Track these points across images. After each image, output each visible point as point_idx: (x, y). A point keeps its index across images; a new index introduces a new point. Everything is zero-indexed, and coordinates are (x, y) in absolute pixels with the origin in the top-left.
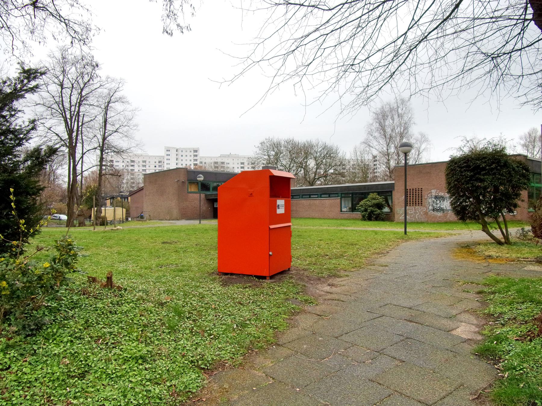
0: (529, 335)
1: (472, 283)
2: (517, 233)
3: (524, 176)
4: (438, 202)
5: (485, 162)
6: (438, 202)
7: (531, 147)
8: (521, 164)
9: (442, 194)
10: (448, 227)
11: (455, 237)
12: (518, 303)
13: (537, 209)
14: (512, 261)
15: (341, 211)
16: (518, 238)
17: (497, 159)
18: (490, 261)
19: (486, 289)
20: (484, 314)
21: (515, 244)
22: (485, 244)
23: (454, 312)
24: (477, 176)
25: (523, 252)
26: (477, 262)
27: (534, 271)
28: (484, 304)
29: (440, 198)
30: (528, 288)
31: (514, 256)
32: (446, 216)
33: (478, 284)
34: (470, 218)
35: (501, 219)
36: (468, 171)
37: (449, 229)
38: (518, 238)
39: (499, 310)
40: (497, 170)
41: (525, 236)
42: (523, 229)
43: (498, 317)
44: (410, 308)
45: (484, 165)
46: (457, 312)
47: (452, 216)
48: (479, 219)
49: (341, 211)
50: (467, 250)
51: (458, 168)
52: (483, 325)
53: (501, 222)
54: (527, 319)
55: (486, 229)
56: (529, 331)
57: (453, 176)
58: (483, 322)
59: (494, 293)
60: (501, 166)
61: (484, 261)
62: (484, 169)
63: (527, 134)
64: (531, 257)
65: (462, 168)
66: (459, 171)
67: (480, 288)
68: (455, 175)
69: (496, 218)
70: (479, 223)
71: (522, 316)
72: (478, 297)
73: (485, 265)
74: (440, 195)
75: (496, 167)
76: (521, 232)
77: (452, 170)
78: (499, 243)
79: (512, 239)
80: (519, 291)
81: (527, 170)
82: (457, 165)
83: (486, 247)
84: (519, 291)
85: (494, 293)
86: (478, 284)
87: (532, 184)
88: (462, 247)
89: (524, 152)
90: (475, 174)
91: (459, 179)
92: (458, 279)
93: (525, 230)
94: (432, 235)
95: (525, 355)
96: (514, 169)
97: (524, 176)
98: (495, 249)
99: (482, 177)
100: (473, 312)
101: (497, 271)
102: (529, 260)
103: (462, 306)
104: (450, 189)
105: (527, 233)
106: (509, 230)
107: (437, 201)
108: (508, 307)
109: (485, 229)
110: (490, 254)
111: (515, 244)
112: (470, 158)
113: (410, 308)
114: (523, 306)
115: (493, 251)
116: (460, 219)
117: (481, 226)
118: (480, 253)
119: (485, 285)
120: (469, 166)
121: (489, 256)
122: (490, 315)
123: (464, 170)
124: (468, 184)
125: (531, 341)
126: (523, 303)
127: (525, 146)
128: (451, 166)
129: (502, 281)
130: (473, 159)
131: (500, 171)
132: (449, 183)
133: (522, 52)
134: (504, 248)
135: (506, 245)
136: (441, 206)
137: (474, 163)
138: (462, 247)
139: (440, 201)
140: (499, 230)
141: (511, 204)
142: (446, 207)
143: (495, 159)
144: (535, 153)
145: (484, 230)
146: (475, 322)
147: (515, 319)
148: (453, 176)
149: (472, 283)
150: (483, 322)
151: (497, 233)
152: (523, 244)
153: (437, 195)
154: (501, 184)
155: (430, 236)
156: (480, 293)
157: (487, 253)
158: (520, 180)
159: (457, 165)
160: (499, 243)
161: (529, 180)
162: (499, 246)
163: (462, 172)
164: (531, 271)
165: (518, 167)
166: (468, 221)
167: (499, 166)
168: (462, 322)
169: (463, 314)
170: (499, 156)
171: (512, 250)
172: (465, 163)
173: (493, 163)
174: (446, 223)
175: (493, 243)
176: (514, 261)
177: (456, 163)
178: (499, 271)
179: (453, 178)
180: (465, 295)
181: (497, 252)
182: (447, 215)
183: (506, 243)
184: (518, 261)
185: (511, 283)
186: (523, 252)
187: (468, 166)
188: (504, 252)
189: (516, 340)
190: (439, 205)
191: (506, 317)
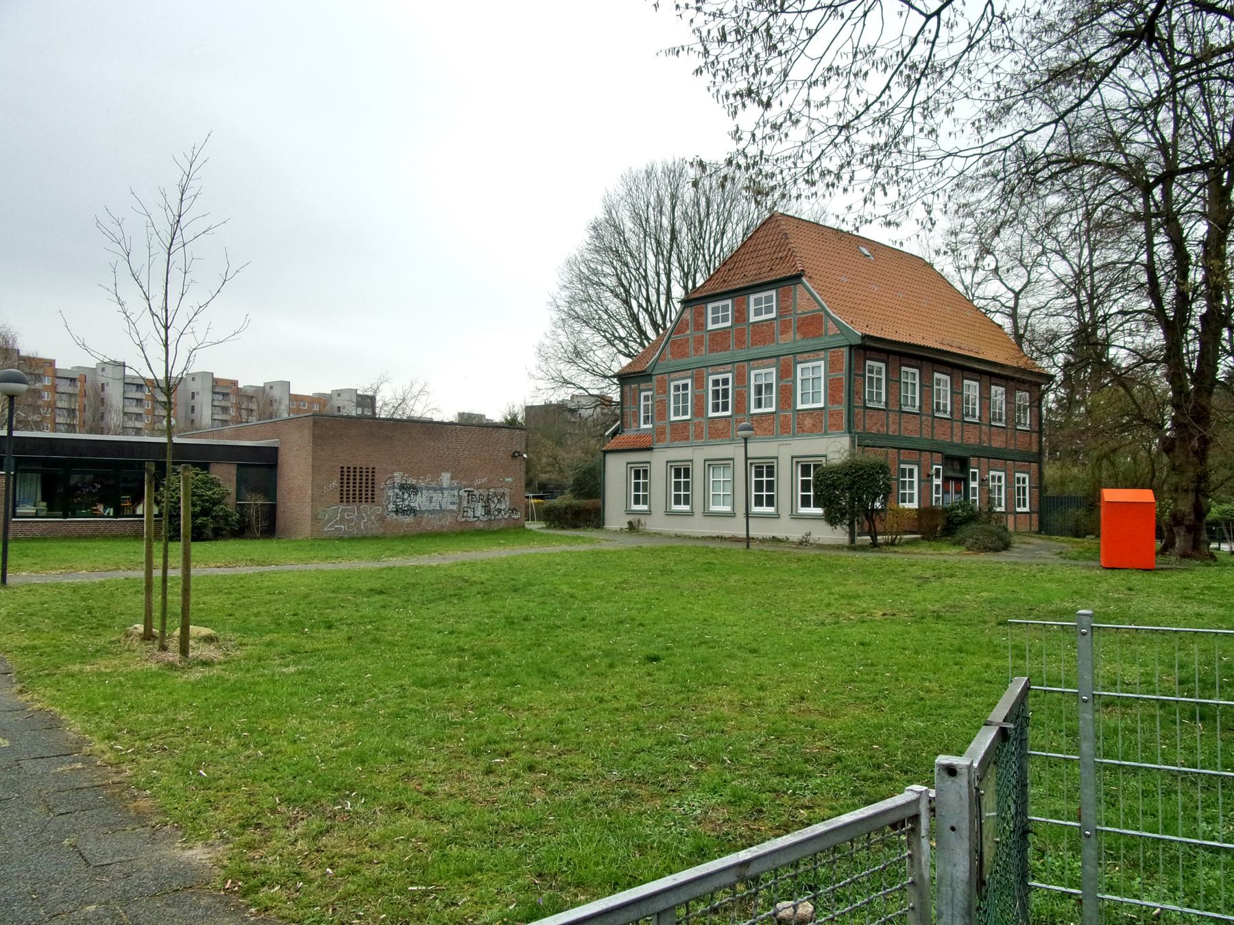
4: (406, 496)
6: (406, 496)
9: (414, 482)
32: (419, 523)
136: (412, 505)
139: (410, 496)
190: (406, 503)
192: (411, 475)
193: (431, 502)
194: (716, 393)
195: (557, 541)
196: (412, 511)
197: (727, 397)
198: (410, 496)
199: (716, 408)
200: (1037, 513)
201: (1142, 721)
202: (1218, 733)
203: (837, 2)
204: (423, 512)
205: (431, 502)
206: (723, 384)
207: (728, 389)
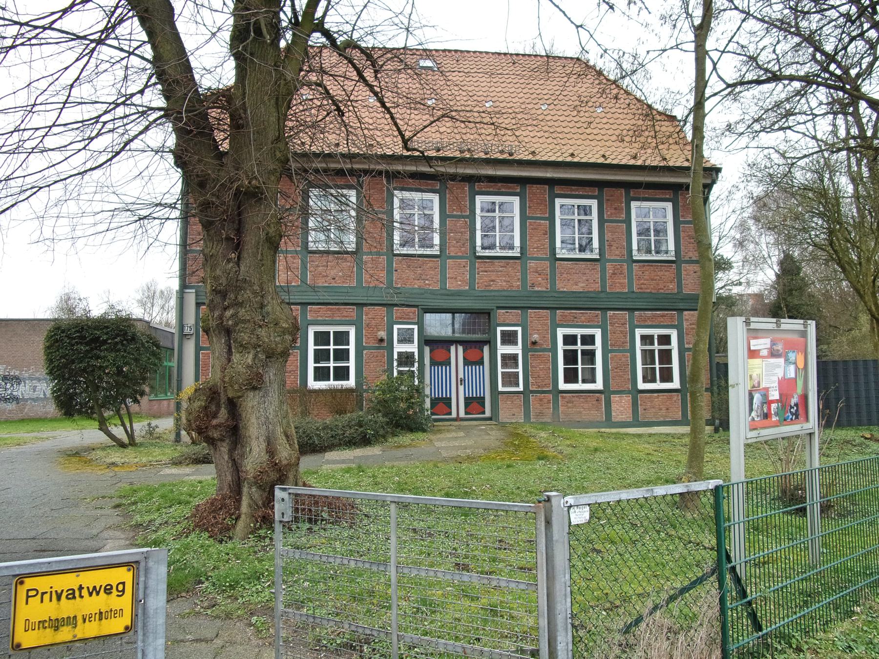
0: (184, 533)
1: (103, 497)
2: (141, 430)
3: (154, 354)
4: (9, 386)
5: (107, 334)
6: (9, 386)
7: (149, 305)
8: (151, 339)
9: (17, 373)
10: (29, 427)
11: (48, 442)
12: (165, 508)
13: (192, 402)
14: (143, 467)
15: (490, 419)
16: (143, 437)
17: (123, 330)
18: (116, 469)
19: (124, 501)
20: (131, 526)
21: (141, 445)
22: (104, 448)
23: (95, 532)
24: (95, 351)
25: (154, 454)
26: (100, 473)
27: (172, 474)
28: (127, 516)
29: (12, 379)
30: (172, 491)
31: (144, 460)
32: (22, 411)
33: (112, 498)
34: (80, 412)
35: (123, 412)
36: (81, 343)
37: (33, 431)
38: (143, 437)
39: (147, 518)
40: (123, 345)
41: (151, 434)
42: (149, 424)
43: (148, 525)
44: (34, 539)
45: (105, 337)
46: (98, 531)
47: (52, 408)
48: (92, 413)
49: (490, 419)
50: (78, 458)
51: (66, 339)
52: (134, 537)
53: (124, 414)
54: (178, 520)
55: (104, 427)
56: (184, 529)
57: (58, 350)
58: (132, 534)
59: (135, 503)
60: (127, 340)
61: (107, 470)
62: (105, 342)
63: (145, 286)
64: (165, 459)
65: (74, 338)
66: (69, 343)
67: (117, 501)
68: (62, 348)
69: (118, 412)
70: (94, 419)
71: (174, 518)
72: (117, 512)
73: (111, 475)
74: (12, 374)
75: (121, 342)
76: (147, 428)
77: (57, 341)
78: (122, 445)
79: (138, 440)
80: (163, 497)
81: (158, 346)
82: (64, 335)
83: (105, 452)
84: (163, 497)
85: (135, 503)
86: (112, 498)
87: (165, 364)
88: (69, 455)
89: (137, 312)
90: (92, 349)
91: (67, 355)
92: (82, 495)
93: (152, 425)
94: (8, 442)
95: (185, 549)
96: (143, 344)
97: (154, 354)
98: (117, 454)
99: (102, 354)
100: (118, 527)
101: (129, 480)
102: (163, 462)
103: (102, 524)
104: (52, 370)
105: (154, 430)
106: (134, 425)
107: (6, 384)
108: (157, 514)
109: (103, 427)
110: (113, 460)
111: (141, 445)
112: (85, 325)
113: (34, 539)
114: (171, 510)
115: (116, 456)
116: (65, 414)
117: (97, 423)
118: (98, 461)
119: (120, 497)
120: (84, 338)
121: (113, 464)
122: (139, 525)
123: (76, 342)
124: (81, 362)
125: (187, 537)
126: (170, 507)
127: (143, 304)
128: (55, 334)
129: (141, 489)
130: (89, 327)
131: (127, 347)
132: (50, 361)
133: (159, 199)
134: (130, 450)
135: (130, 448)
136: (14, 393)
137: (92, 334)
138: (69, 455)
139: (12, 385)
140: (122, 428)
141: (136, 392)
142: (22, 394)
143: (120, 331)
144: (154, 315)
145: (101, 429)
146: (123, 536)
147: (166, 522)
148: (58, 350)
149: (103, 497)
150: (132, 534)
151: (119, 432)
152: (152, 445)
153: (7, 374)
154: (126, 364)
155: (5, 444)
156: (117, 506)
157: (109, 460)
158: (149, 359)
159: (64, 335)
160: (122, 445)
161: (160, 359)
162: (122, 449)
163: (73, 345)
164: (168, 475)
165: (147, 342)
166: (76, 417)
167: (125, 340)
168: (107, 539)
169: (105, 532)
170: (125, 326)
171: (140, 452)
172: (78, 332)
173: (117, 335)
174: (22, 420)
175: (114, 446)
176: (145, 466)
177: (63, 332)
178: (132, 480)
179: (57, 353)
180: (99, 512)
181: (122, 458)
182: (24, 408)
183: (130, 444)
184: (151, 465)
185: (151, 492)
186: (154, 454)
187: (83, 338)
188: (130, 456)
189: (174, 539)
190: (9, 392)
191: (157, 523)
192: (15, 367)
193: (34, 391)
194: (648, 356)
195: (726, 644)
196: (16, 399)
197: (644, 352)
198: (12, 385)
199: (649, 377)
200: (149, 42)
201: (442, 403)
202: (652, 227)
203: (838, 3)
204: (24, 399)
205: (34, 391)
206: (652, 344)
207: (669, 352)
